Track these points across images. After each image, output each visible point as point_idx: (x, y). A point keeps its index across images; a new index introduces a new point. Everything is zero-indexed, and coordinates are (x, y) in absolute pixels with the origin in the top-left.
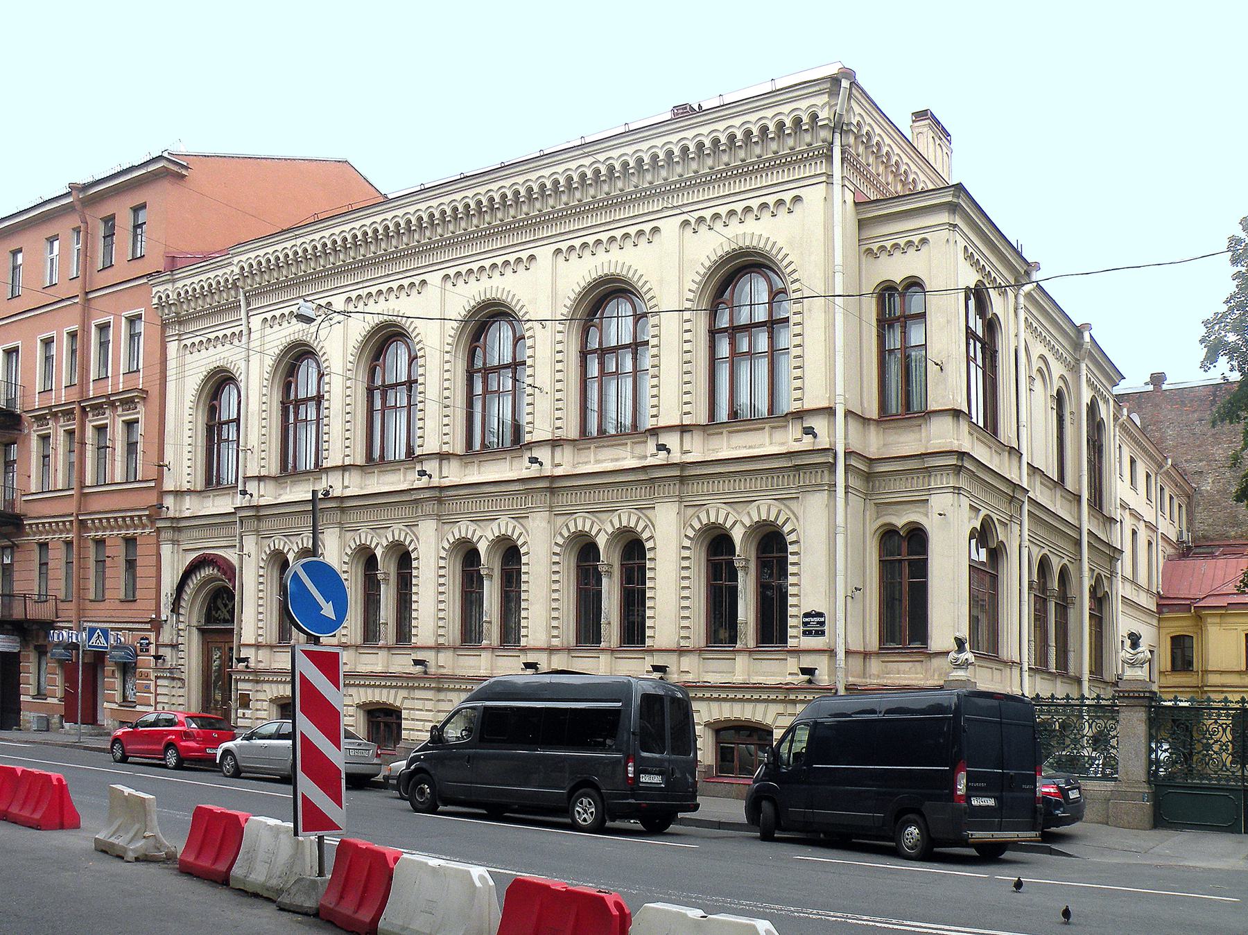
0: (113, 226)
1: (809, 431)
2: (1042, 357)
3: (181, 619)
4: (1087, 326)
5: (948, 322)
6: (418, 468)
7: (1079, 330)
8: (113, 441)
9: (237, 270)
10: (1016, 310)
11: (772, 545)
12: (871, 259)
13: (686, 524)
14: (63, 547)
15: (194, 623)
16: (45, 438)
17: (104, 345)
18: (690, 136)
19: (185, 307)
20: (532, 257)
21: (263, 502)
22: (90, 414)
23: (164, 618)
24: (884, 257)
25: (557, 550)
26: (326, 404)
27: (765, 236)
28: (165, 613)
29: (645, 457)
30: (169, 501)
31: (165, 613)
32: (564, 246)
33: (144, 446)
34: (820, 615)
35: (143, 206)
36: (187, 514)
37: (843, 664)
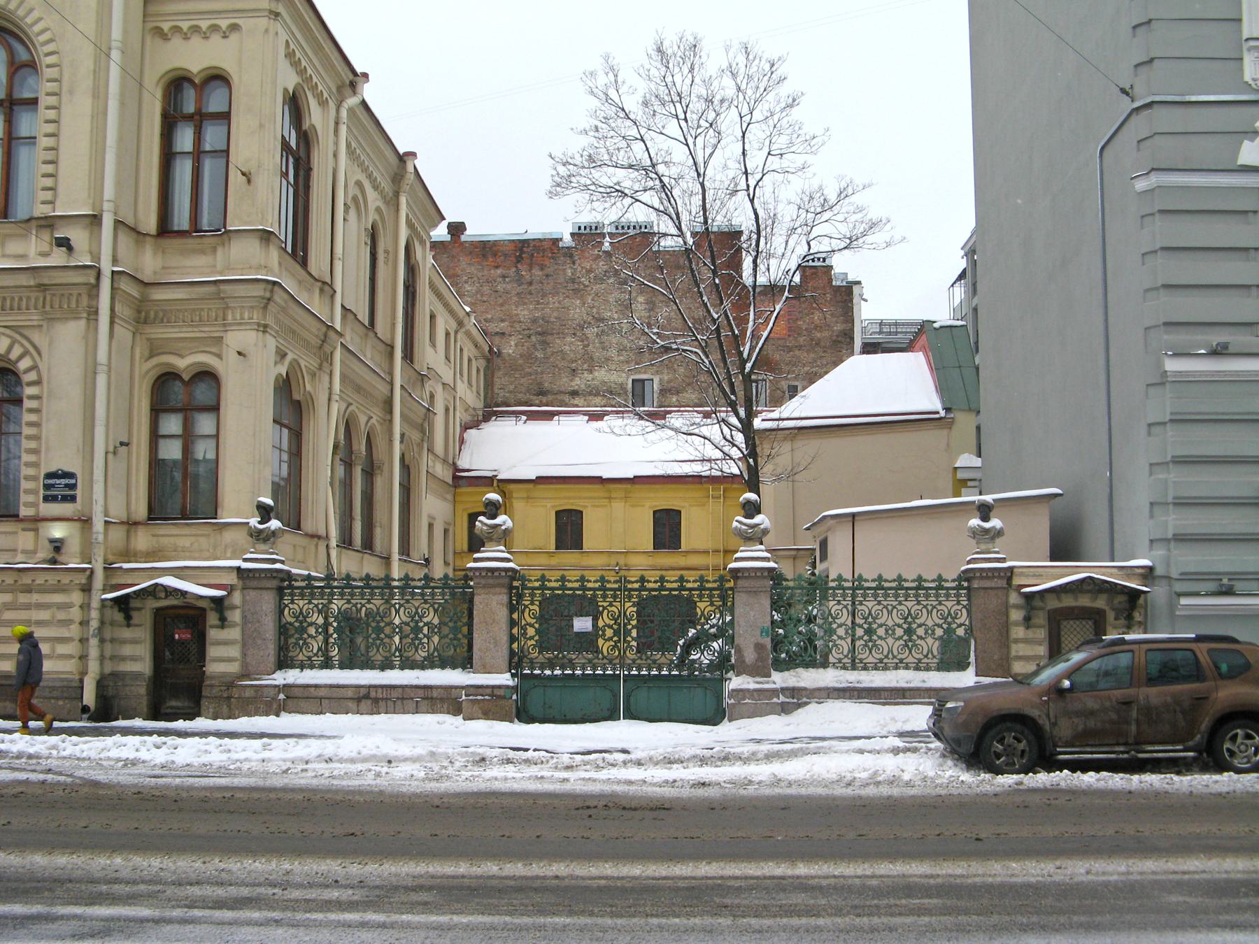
1: (64, 243)
2: (359, 184)
4: (413, 154)
5: (261, 126)
7: (404, 158)
10: (337, 123)
12: (159, 41)
24: (177, 41)
34: (71, 475)
37: (101, 538)
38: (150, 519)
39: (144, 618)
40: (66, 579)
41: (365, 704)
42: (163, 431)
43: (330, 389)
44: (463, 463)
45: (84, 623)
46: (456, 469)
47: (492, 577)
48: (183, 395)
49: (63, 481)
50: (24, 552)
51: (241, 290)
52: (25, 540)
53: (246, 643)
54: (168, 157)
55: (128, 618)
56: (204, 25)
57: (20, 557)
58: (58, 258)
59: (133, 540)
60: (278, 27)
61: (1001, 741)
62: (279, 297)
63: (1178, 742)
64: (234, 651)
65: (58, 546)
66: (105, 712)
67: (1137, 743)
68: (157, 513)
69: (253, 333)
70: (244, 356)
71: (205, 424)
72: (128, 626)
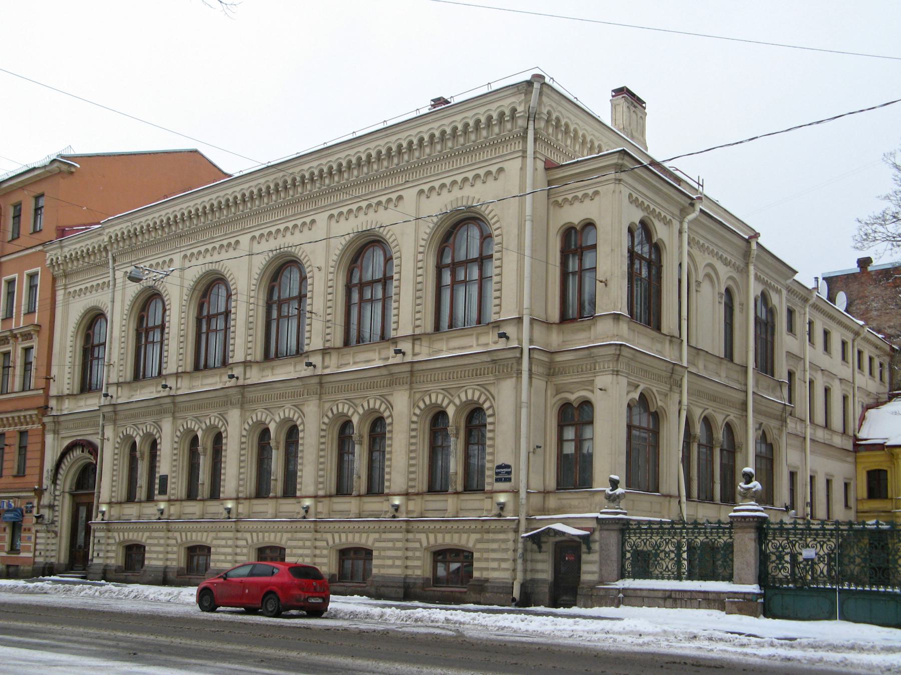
0: (20, 210)
1: (503, 335)
3: (58, 487)
6: (230, 373)
8: (14, 362)
9: (106, 239)
11: (475, 419)
13: (415, 405)
14: (18, 436)
15: (67, 489)
18: (447, 124)
19: (70, 265)
20: (313, 221)
21: (120, 401)
22: (20, 339)
23: (44, 487)
25: (324, 427)
26: (233, 316)
27: (477, 197)
28: (47, 483)
29: (388, 359)
30: (53, 403)
31: (47, 483)
32: (335, 212)
34: (508, 467)
35: (42, 195)
37: (524, 501)
38: (557, 489)
39: (548, 547)
40: (505, 525)
41: (669, 602)
42: (565, 438)
43: (680, 402)
44: (861, 435)
45: (515, 551)
46: (856, 438)
47: (745, 522)
48: (575, 415)
49: (505, 470)
50: (487, 510)
51: (602, 351)
52: (487, 504)
53: (602, 563)
54: (565, 275)
55: (540, 547)
57: (485, 513)
58: (502, 344)
59: (547, 503)
60: (622, 187)
62: (625, 352)
64: (595, 568)
65: (502, 506)
66: (526, 600)
68: (562, 485)
69: (610, 376)
70: (605, 390)
71: (587, 433)
72: (540, 552)
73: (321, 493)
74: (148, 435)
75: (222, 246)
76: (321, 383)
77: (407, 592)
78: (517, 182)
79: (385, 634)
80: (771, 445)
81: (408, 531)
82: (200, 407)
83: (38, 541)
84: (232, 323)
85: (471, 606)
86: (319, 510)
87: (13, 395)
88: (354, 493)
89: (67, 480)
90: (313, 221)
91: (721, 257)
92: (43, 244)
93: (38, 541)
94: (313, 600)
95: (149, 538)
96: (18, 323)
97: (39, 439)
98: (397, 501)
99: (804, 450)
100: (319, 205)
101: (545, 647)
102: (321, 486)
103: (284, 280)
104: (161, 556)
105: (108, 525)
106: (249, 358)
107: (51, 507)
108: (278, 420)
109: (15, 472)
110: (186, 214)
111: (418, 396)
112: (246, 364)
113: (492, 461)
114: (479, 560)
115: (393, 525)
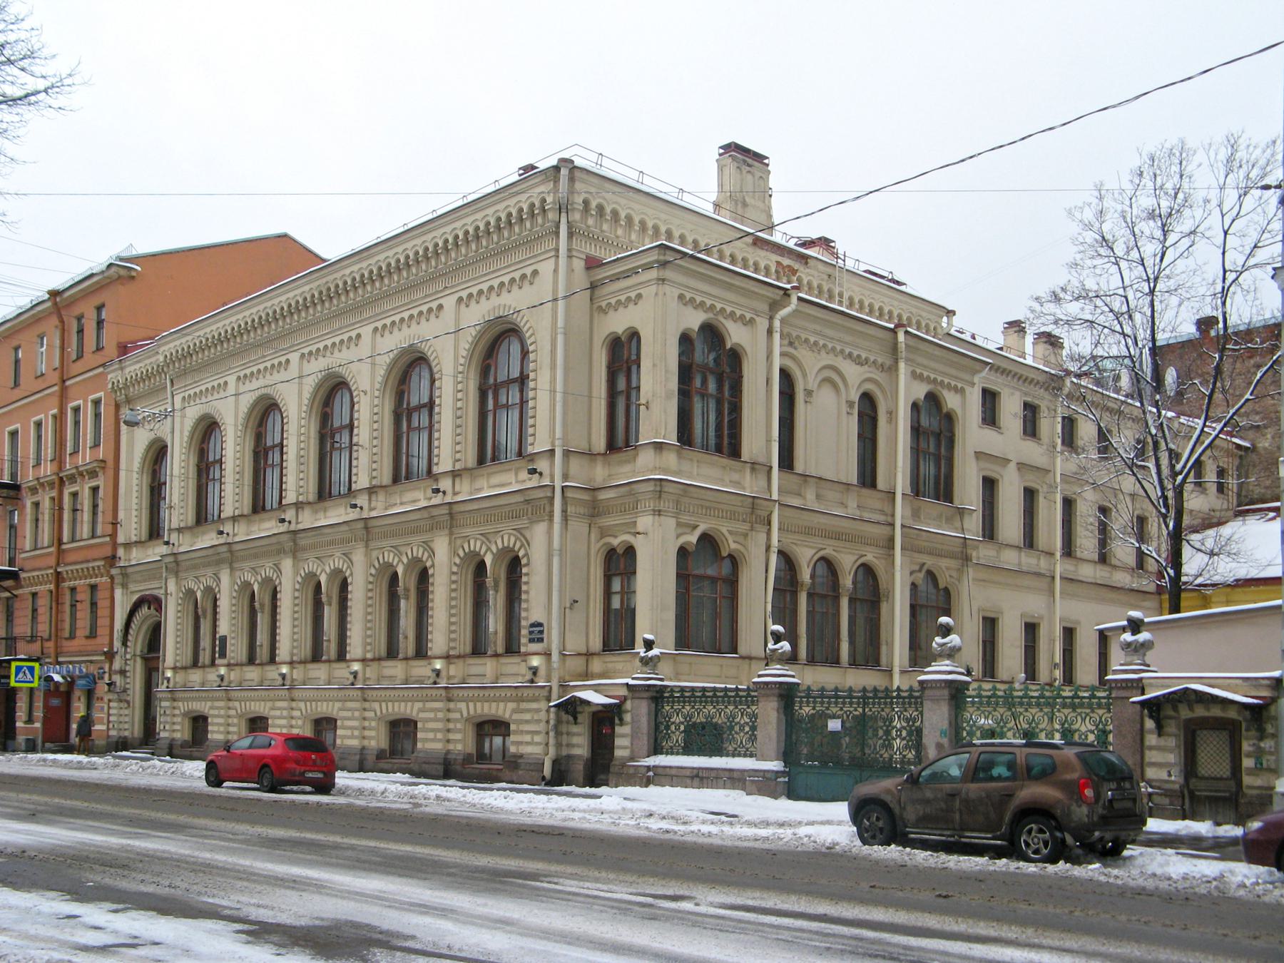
8: (82, 504)
9: (161, 358)
12: (602, 315)
14: (89, 592)
15: (138, 652)
16: (37, 505)
17: (77, 423)
26: (531, 385)
28: (117, 644)
31: (117, 644)
33: (105, 506)
34: (540, 625)
35: (103, 305)
36: (133, 563)
39: (584, 718)
41: (696, 781)
45: (548, 722)
48: (620, 563)
53: (634, 736)
56: (623, 298)
58: (534, 482)
61: (878, 819)
62: (668, 488)
63: (986, 831)
65: (535, 671)
66: (559, 777)
67: (962, 830)
68: (607, 647)
73: (369, 656)
74: (416, 561)
75: (273, 366)
76: (366, 528)
77: (448, 770)
78: (550, 288)
79: (381, 811)
80: (947, 590)
81: (449, 700)
82: (256, 556)
83: (112, 712)
84: (531, 394)
85: (503, 785)
86: (452, 673)
87: (82, 543)
88: (401, 656)
89: (138, 642)
90: (535, 273)
91: (850, 355)
92: (103, 365)
93: (112, 712)
94: (310, 775)
95: (211, 708)
96: (84, 458)
97: (107, 594)
98: (438, 665)
99: (1052, 592)
100: (365, 315)
101: (464, 821)
102: (369, 648)
103: (502, 357)
104: (439, 736)
105: (173, 695)
106: (301, 499)
107: (123, 672)
108: (328, 570)
109: (87, 633)
110: (451, 240)
111: (459, 542)
112: (298, 506)
113: (526, 618)
114: (516, 732)
115: (434, 692)
